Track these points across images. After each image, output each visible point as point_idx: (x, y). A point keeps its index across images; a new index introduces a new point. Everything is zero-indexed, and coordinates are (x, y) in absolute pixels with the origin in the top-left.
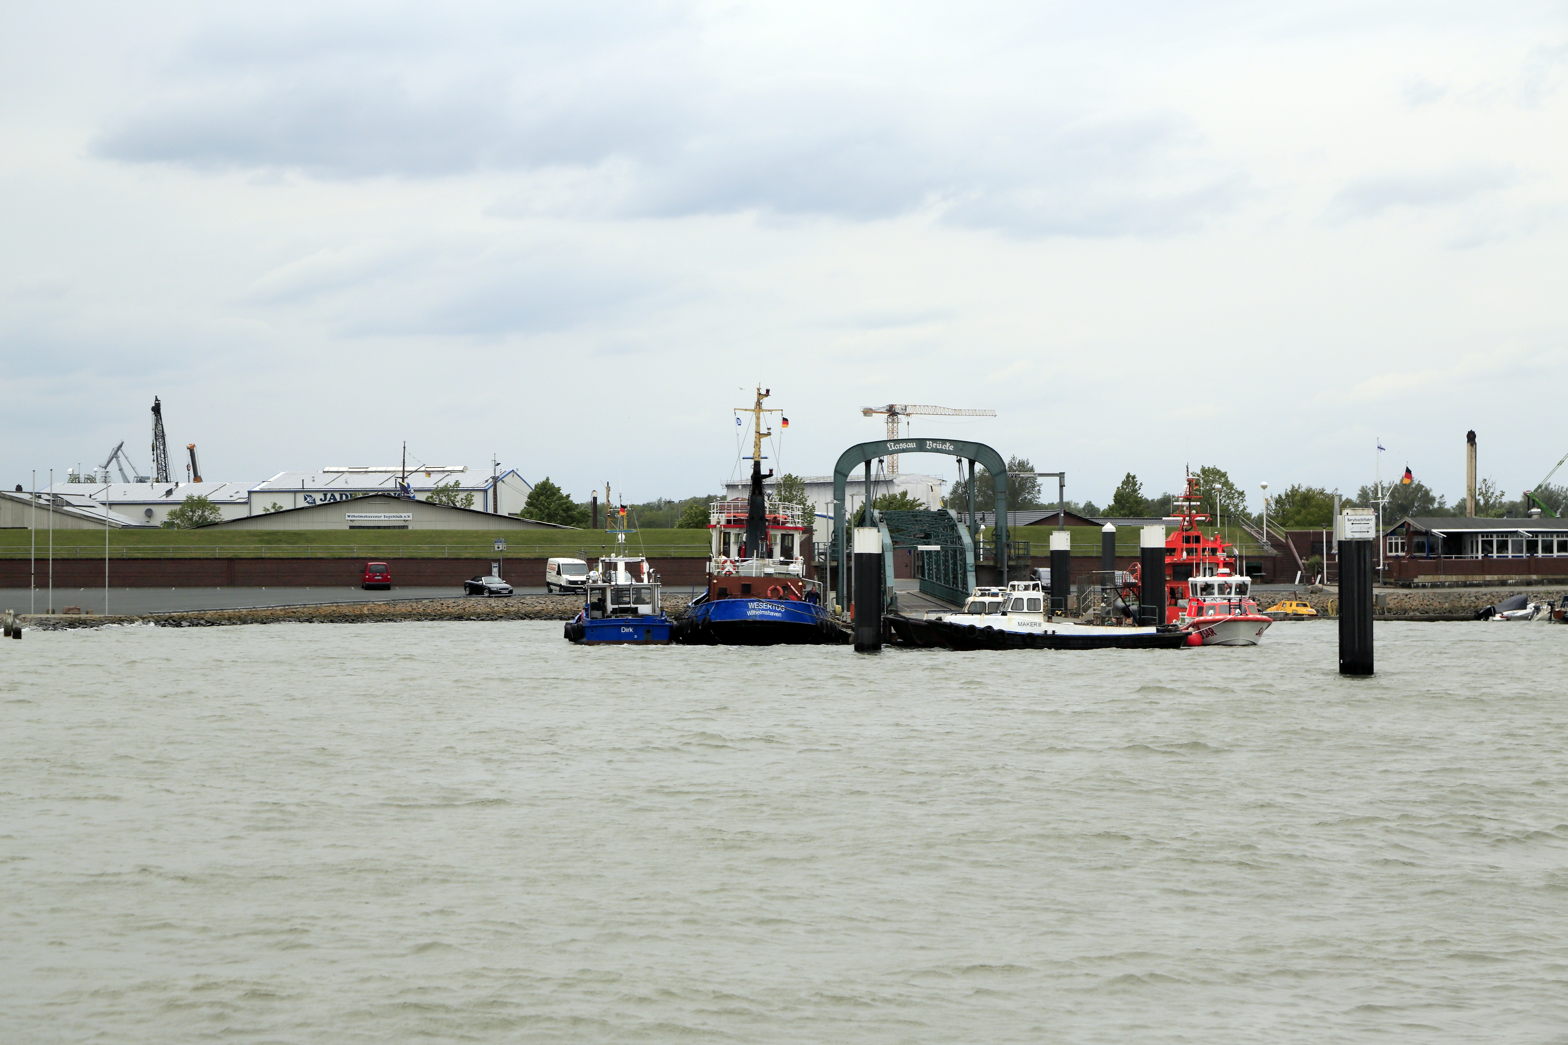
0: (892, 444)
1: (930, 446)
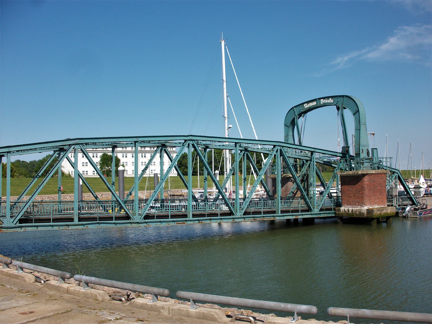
0: (306, 104)
1: (322, 102)
